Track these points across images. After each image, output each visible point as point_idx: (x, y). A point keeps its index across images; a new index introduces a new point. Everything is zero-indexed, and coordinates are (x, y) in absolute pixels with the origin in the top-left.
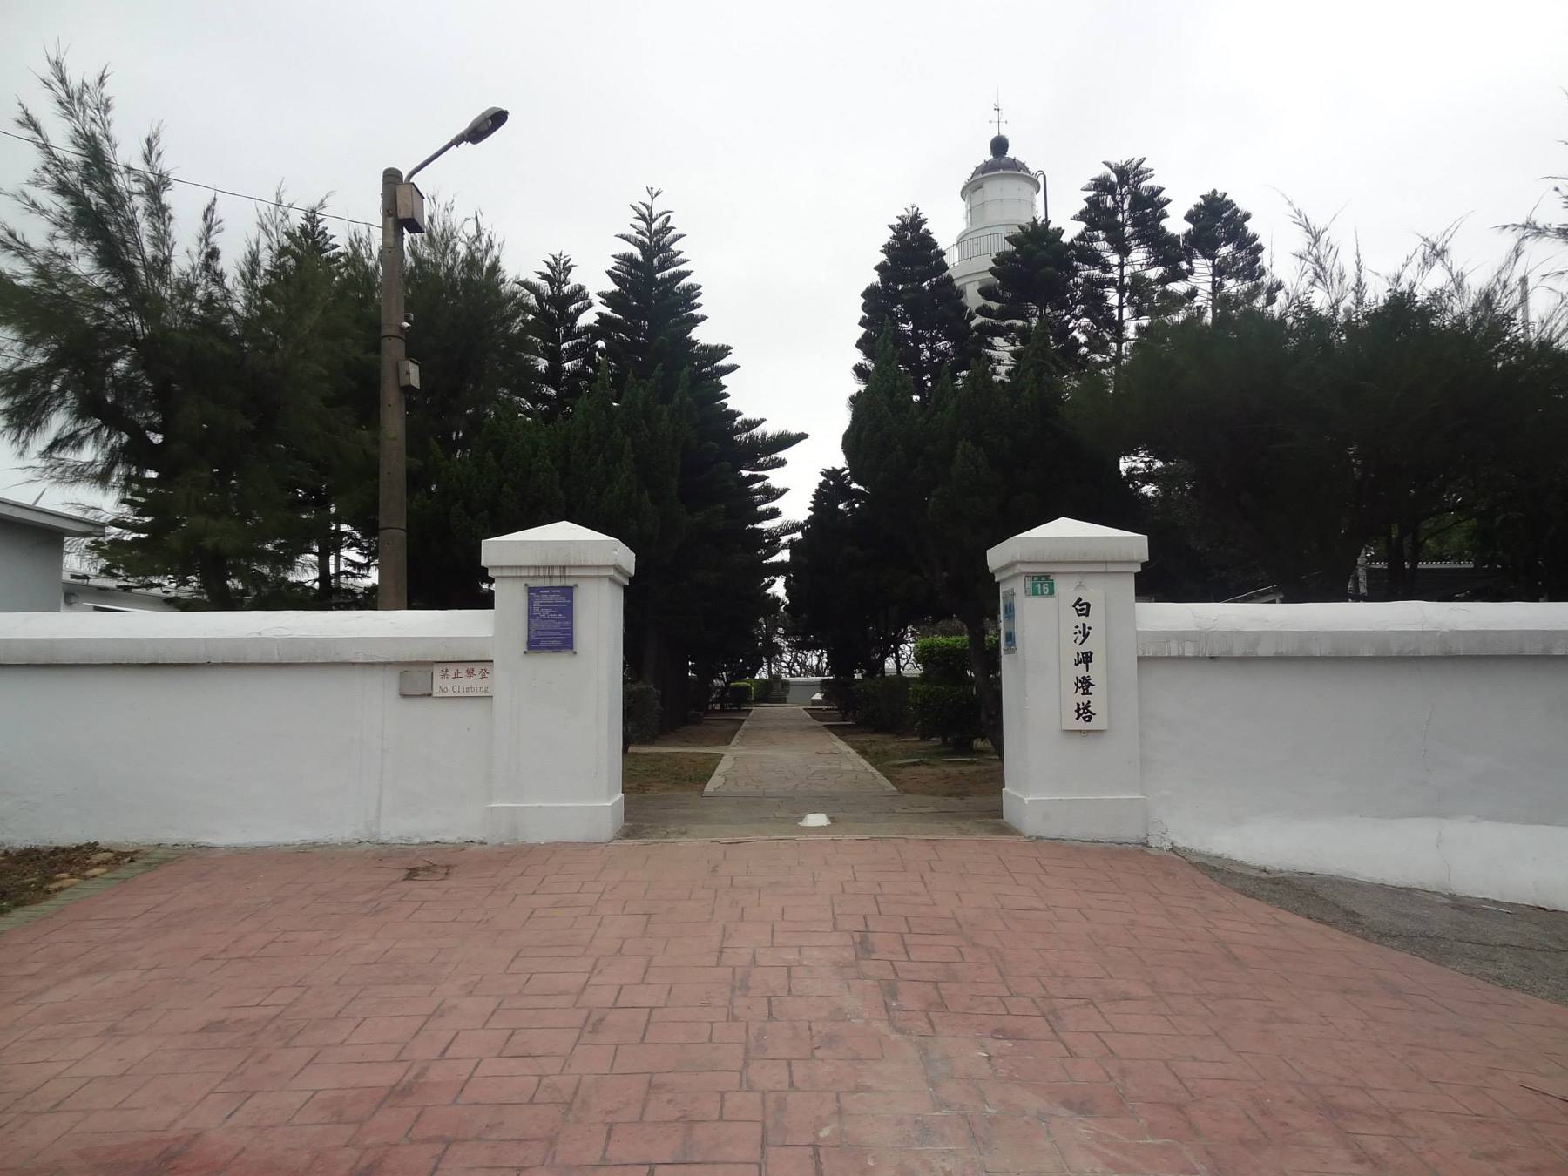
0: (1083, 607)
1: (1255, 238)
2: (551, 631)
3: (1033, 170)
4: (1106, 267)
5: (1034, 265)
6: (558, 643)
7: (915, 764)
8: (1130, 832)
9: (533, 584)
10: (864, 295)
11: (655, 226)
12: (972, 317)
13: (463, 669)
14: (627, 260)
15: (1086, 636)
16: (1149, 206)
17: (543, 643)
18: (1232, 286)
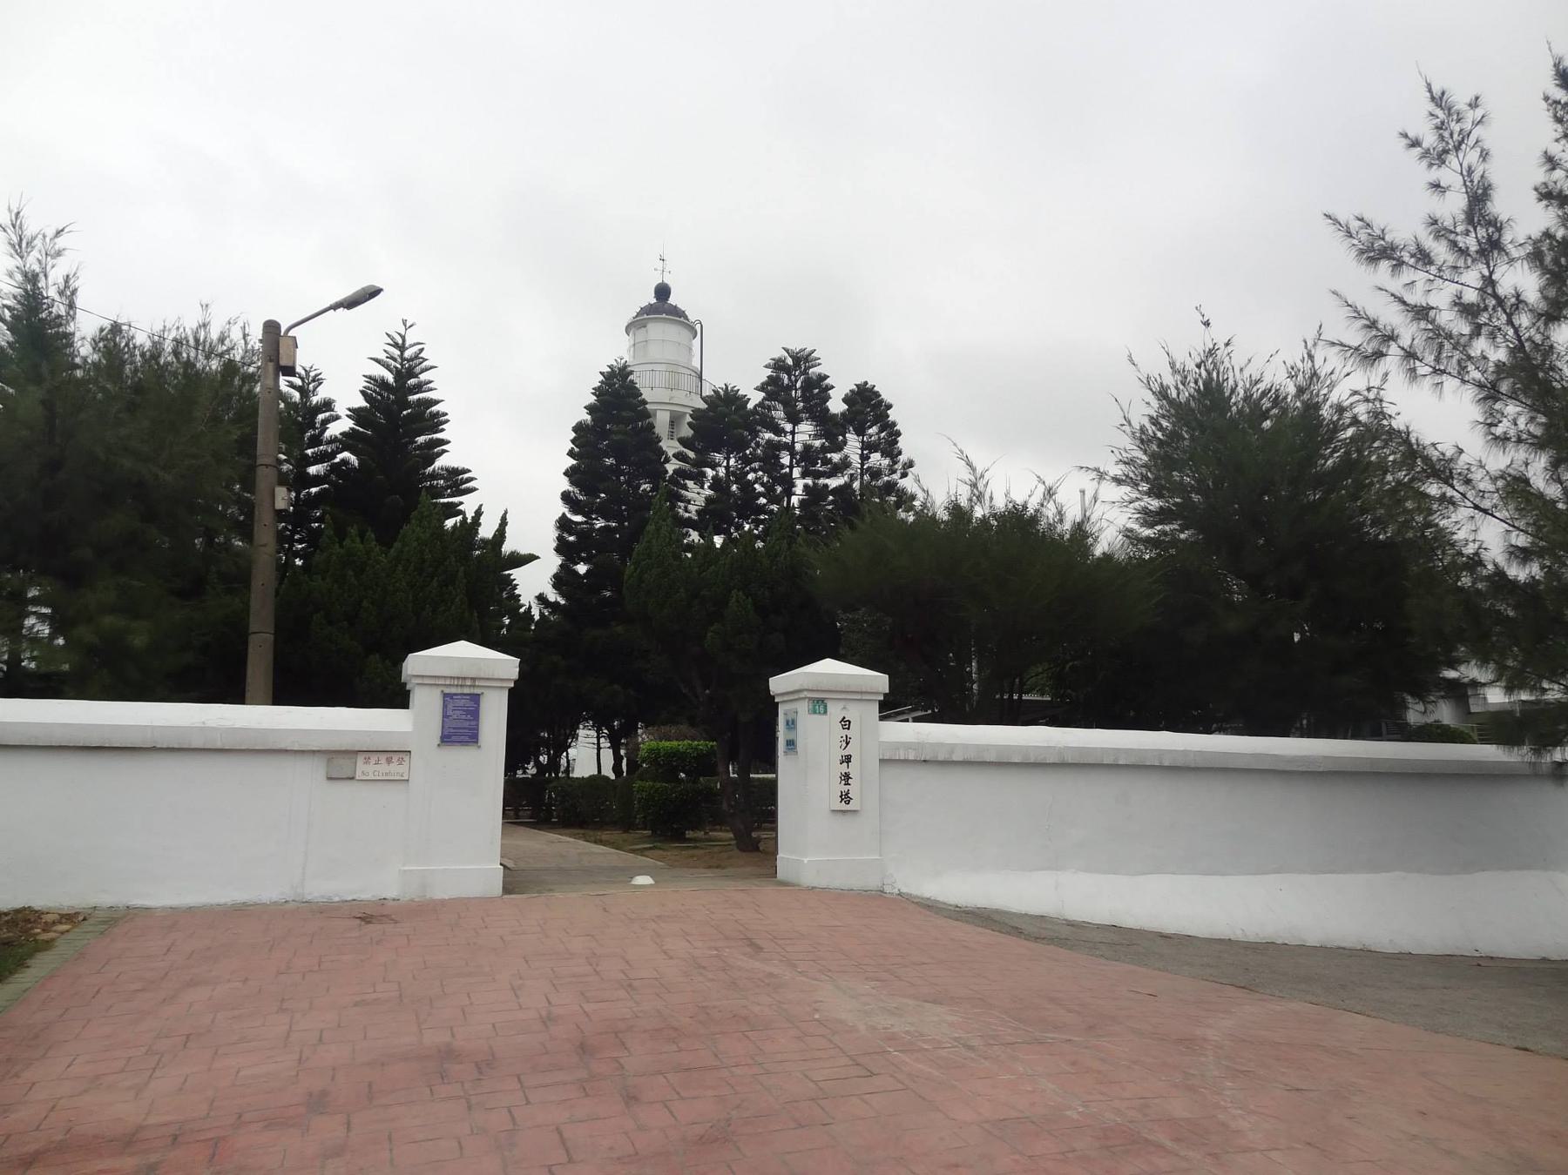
0: (846, 724)
1: (894, 424)
2: (459, 729)
3: (692, 318)
4: (779, 431)
5: (722, 422)
8: (873, 883)
9: (447, 691)
10: (575, 429)
11: (407, 354)
12: (667, 460)
13: (383, 757)
14: (382, 384)
16: (817, 389)
18: (876, 458)
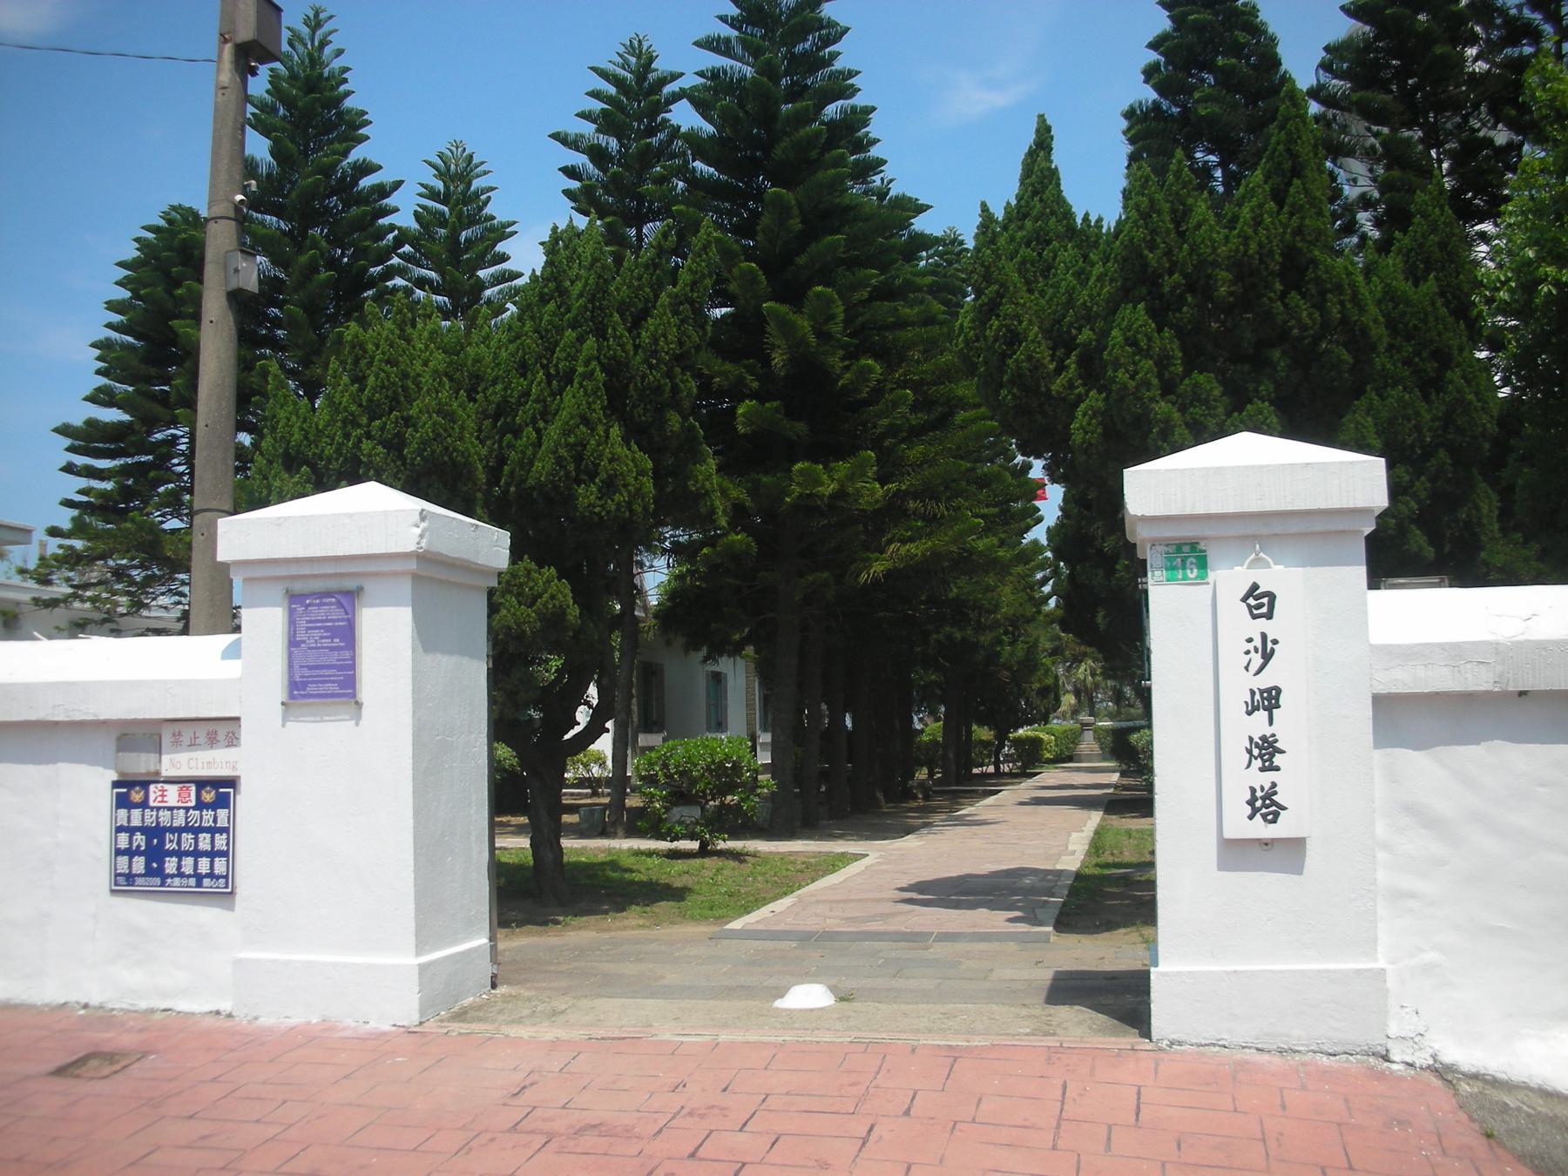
0: (1261, 602)
6: (334, 688)
7: (640, 926)
9: (298, 587)
15: (1267, 656)
17: (311, 689)
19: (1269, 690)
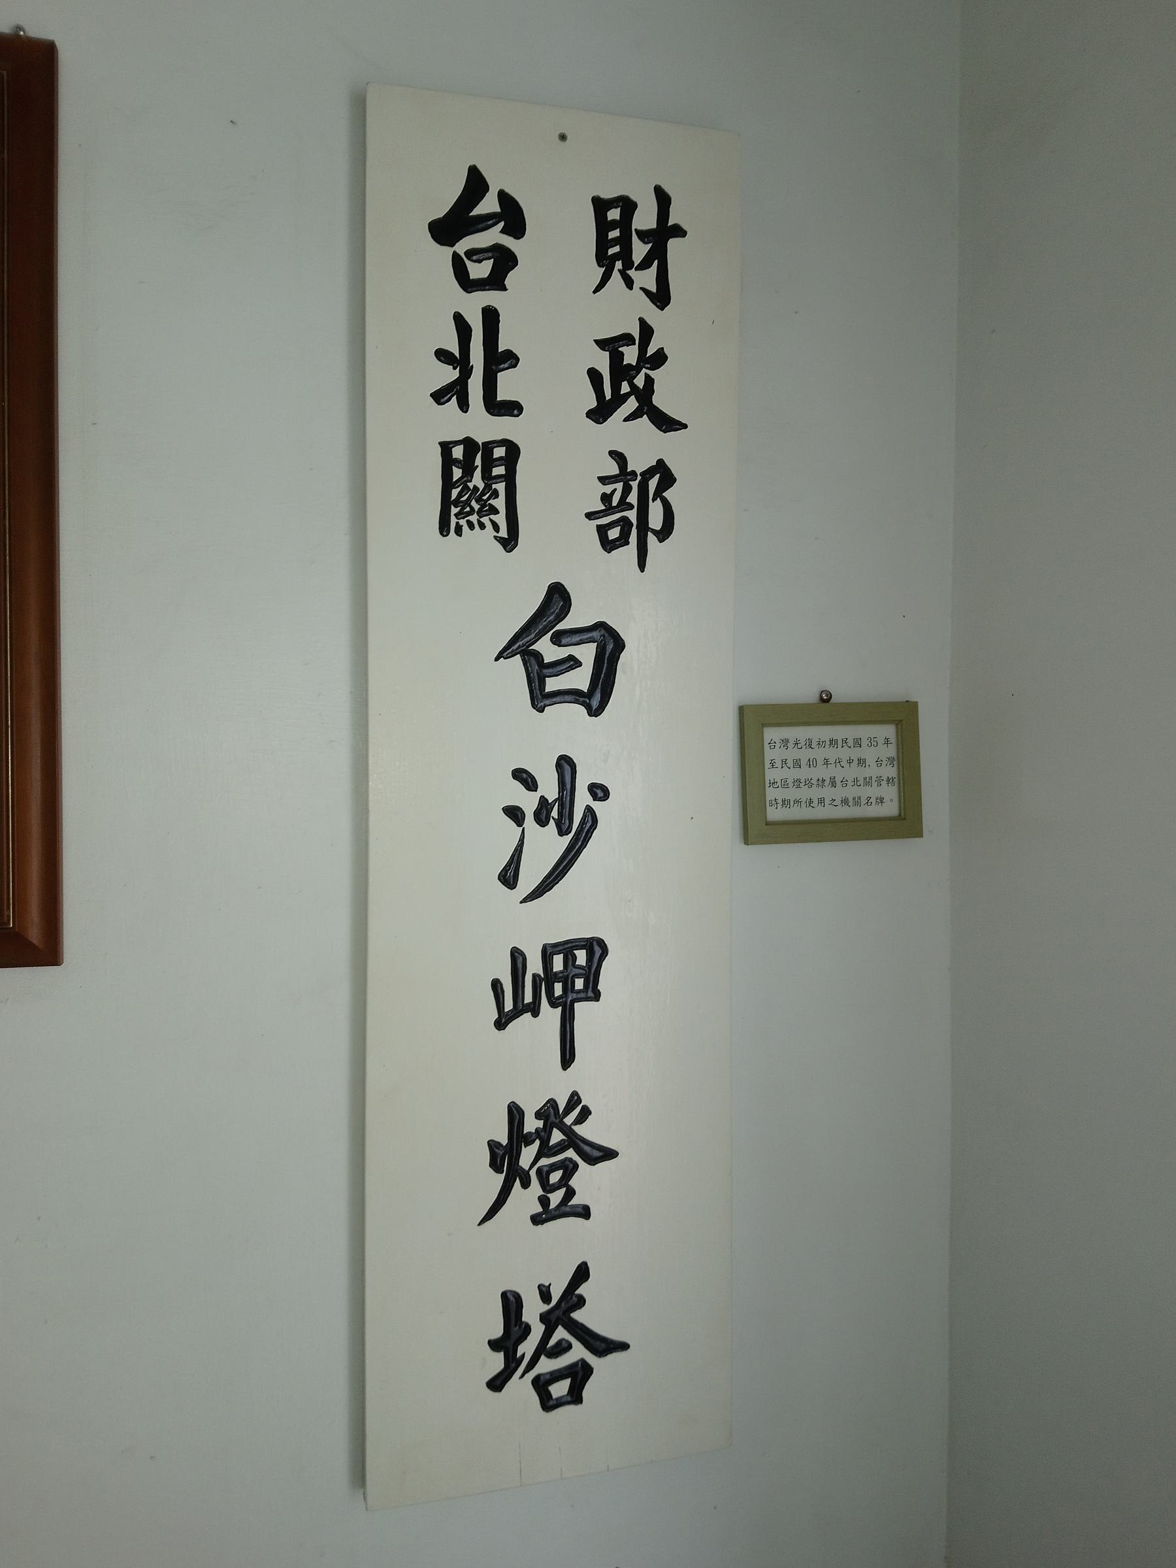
19: (567, 948)
